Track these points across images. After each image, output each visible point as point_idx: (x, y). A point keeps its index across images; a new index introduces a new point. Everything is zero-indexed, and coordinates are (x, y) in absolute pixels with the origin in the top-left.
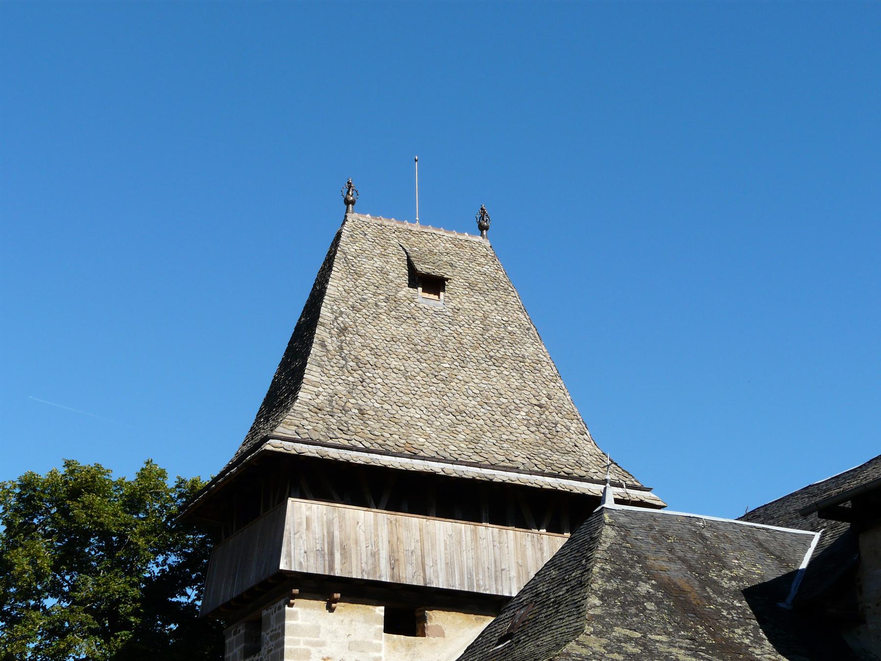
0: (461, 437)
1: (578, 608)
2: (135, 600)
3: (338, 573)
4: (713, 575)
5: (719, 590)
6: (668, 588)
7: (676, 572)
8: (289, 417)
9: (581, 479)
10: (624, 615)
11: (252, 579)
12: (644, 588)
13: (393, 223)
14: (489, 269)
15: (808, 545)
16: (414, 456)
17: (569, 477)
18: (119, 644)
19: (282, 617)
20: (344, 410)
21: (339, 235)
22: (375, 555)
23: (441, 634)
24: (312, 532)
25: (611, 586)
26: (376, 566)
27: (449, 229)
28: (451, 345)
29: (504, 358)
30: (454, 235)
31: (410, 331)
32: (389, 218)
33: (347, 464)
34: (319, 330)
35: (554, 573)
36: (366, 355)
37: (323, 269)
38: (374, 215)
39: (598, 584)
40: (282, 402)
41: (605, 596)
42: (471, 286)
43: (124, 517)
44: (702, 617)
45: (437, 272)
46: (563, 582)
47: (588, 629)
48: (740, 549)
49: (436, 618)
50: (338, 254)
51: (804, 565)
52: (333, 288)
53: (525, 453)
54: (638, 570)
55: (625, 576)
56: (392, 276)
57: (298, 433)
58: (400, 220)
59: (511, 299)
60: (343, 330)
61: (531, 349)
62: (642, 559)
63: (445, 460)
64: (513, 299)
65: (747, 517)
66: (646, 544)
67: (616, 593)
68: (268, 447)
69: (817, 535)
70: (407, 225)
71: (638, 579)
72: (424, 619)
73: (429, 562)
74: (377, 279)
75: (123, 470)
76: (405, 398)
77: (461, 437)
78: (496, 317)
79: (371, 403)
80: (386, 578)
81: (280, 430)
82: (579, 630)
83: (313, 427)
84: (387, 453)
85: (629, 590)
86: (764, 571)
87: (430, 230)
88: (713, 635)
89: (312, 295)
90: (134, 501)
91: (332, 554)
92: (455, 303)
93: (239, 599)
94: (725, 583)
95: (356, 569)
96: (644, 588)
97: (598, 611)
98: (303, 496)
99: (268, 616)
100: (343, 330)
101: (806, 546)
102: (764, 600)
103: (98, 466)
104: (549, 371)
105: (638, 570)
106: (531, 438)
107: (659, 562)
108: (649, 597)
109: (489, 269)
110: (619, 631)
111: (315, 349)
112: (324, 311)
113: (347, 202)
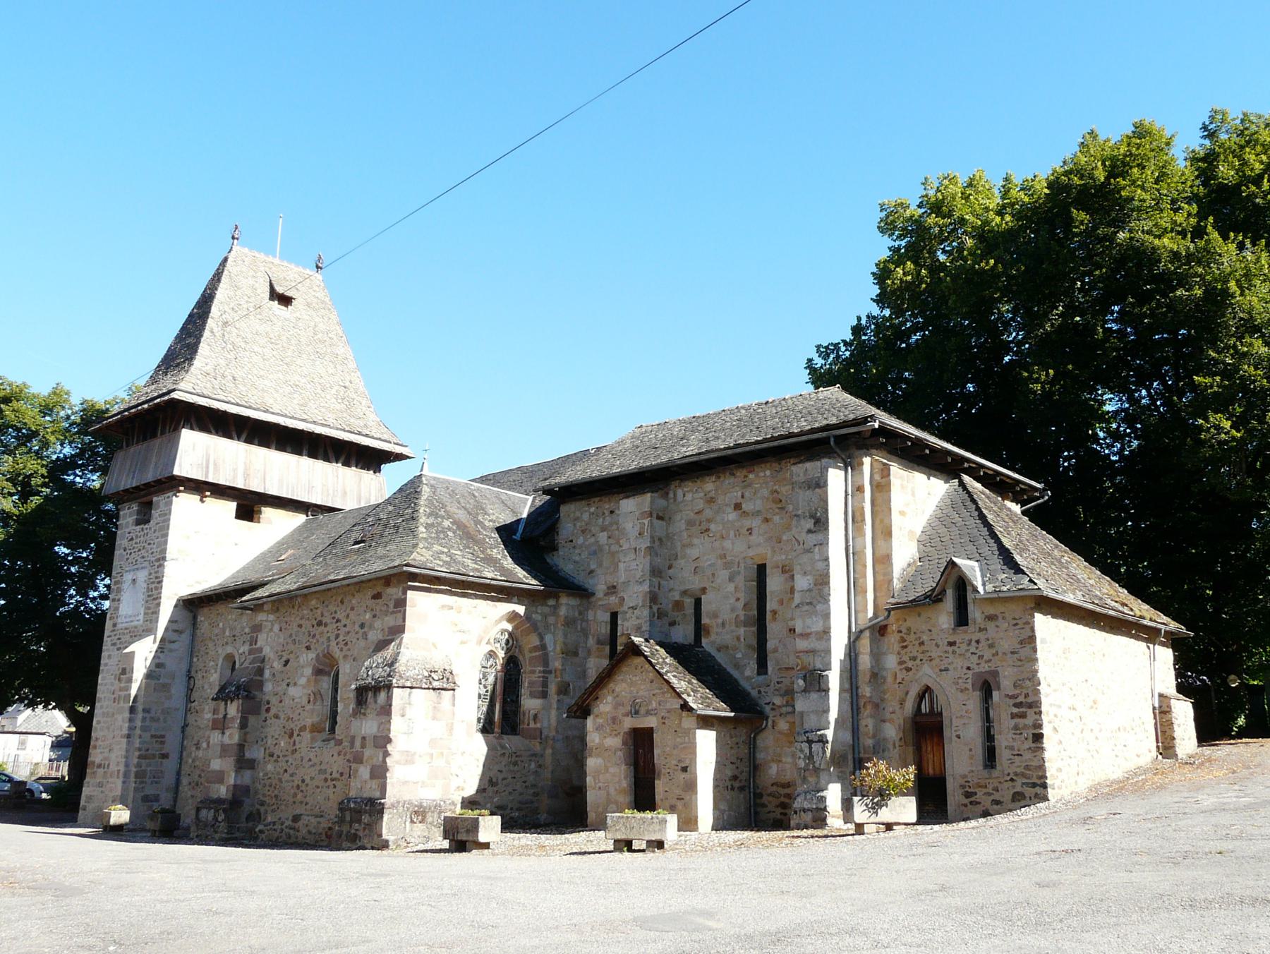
0: (296, 401)
1: (413, 532)
2: (43, 476)
3: (210, 480)
4: (480, 518)
5: (484, 527)
6: (459, 524)
7: (462, 516)
8: (188, 377)
9: (367, 436)
10: (438, 538)
11: (150, 477)
12: (447, 523)
13: (262, 256)
14: (321, 295)
15: (525, 504)
16: (267, 411)
17: (360, 434)
18: (33, 505)
19: (170, 503)
20: (223, 376)
21: (226, 260)
22: (235, 470)
23: (270, 522)
24: (195, 452)
25: (430, 521)
26: (235, 477)
27: (297, 265)
28: (293, 342)
29: (325, 354)
30: (301, 269)
31: (268, 329)
32: (259, 251)
33: (225, 413)
34: (210, 321)
35: (390, 508)
36: (239, 342)
37: (213, 279)
38: (251, 249)
39: (423, 519)
40: (178, 365)
41: (428, 526)
42: (308, 305)
43: (40, 420)
44: (476, 542)
45: (288, 294)
46: (399, 515)
47: (421, 545)
48: (493, 504)
49: (268, 513)
50: (226, 272)
51: (525, 515)
52: (221, 294)
53: (334, 416)
54: (442, 513)
55: (437, 516)
56: (259, 291)
57: (192, 386)
58: (267, 254)
59: (332, 317)
60: (226, 324)
61: (343, 350)
62: (444, 506)
63: (286, 416)
64: (334, 317)
65: (483, 479)
66: (446, 498)
67: (432, 525)
68: (174, 395)
69: (531, 498)
70: (270, 259)
71: (443, 517)
72: (260, 512)
73: (268, 478)
74: (249, 292)
75: (40, 387)
76: (262, 373)
77: (296, 401)
78: (322, 326)
79: (240, 374)
80: (241, 486)
81: (182, 385)
82: (415, 546)
83: (204, 386)
84: (250, 407)
85: (439, 524)
86: (506, 518)
87: (285, 264)
88: (482, 552)
89: (203, 295)
90: (46, 409)
91: (207, 467)
92: (298, 314)
93: (137, 488)
94: (487, 523)
95: (222, 480)
96: (447, 523)
97: (424, 535)
98: (192, 429)
99: (158, 502)
100: (226, 324)
101: (525, 504)
102: (506, 532)
103: (24, 384)
104: (352, 365)
105: (442, 513)
106: (338, 407)
107: (453, 508)
108: (449, 529)
109: (321, 295)
110: (437, 548)
111: (206, 334)
112: (214, 309)
113: (233, 238)
